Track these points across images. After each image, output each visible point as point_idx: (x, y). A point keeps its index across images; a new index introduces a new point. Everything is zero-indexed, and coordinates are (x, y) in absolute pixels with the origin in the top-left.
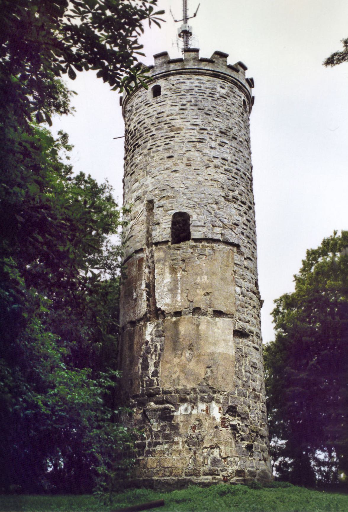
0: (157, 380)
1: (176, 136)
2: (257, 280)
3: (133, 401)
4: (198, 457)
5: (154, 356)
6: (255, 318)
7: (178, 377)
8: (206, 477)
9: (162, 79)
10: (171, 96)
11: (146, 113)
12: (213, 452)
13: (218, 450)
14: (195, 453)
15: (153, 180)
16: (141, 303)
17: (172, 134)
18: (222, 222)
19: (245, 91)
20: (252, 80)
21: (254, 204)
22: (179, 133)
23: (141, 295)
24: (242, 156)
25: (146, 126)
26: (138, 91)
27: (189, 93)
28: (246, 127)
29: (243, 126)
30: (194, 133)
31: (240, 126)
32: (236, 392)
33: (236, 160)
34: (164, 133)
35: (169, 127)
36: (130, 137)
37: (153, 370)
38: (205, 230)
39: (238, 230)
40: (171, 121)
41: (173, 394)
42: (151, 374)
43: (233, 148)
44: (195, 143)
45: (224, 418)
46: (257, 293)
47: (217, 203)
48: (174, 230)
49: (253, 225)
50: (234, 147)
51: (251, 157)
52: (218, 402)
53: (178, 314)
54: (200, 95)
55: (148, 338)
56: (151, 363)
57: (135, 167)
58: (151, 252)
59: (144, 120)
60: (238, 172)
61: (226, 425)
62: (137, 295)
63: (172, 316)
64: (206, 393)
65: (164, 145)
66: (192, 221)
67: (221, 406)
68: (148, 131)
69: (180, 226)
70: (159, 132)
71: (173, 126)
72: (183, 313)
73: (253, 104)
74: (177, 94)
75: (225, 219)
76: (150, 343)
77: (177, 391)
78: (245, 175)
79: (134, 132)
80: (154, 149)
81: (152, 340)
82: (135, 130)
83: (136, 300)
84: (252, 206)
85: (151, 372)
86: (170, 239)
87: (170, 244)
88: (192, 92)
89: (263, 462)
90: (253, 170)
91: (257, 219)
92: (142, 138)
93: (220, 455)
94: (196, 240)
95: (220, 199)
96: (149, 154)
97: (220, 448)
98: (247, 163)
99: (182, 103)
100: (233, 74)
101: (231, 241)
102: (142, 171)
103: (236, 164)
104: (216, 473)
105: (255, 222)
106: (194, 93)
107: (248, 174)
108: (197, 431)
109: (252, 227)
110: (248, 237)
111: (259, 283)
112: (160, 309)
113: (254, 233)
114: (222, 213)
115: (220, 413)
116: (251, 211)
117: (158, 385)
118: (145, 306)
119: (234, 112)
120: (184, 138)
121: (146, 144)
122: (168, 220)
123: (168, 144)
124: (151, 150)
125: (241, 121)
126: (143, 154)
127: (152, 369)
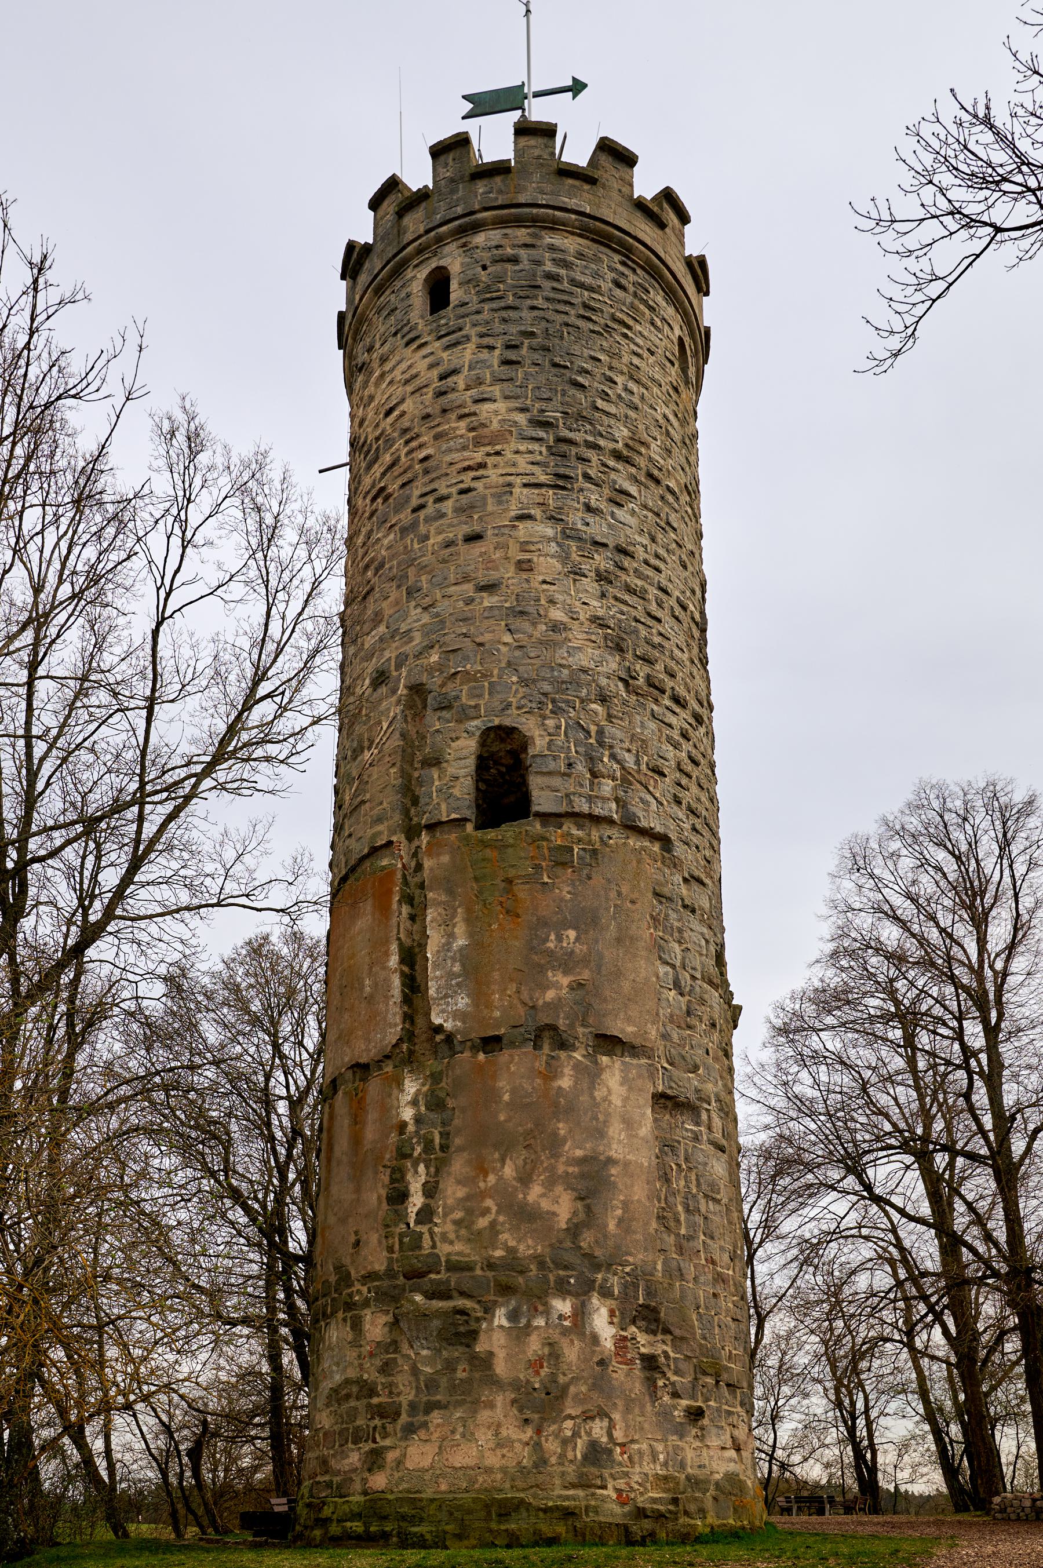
0: (431, 1233)
1: (490, 461)
2: (723, 946)
3: (365, 1289)
4: (547, 1440)
5: (421, 1168)
6: (716, 1059)
7: (493, 1224)
8: (571, 1492)
9: (455, 244)
10: (478, 312)
11: (407, 376)
12: (591, 1428)
13: (605, 1423)
14: (539, 1432)
15: (426, 619)
16: (387, 1011)
17: (478, 456)
18: (618, 762)
19: (682, 304)
20: (702, 261)
21: (711, 708)
22: (498, 453)
23: (387, 981)
24: (674, 545)
25: (407, 424)
26: (387, 293)
27: (529, 302)
28: (688, 442)
29: (677, 437)
30: (541, 453)
31: (668, 433)
32: (659, 1267)
33: (657, 556)
34: (458, 450)
35: (472, 429)
36: (363, 465)
37: (419, 1205)
38: (570, 786)
39: (664, 787)
40: (474, 408)
41: (478, 1272)
42: (413, 1215)
43: (650, 514)
44: (543, 491)
45: (625, 1338)
46: (720, 983)
47: (603, 699)
48: (482, 786)
49: (707, 776)
50: (651, 510)
51: (701, 549)
52: (606, 1293)
53: (491, 1043)
54: (557, 311)
55: (407, 1114)
56: (416, 1185)
57: (377, 570)
58: (415, 855)
59: (403, 401)
60: (664, 597)
61: (629, 1356)
62: (376, 985)
63: (475, 1049)
64: (573, 1269)
65: (455, 496)
66: (534, 756)
67: (612, 1303)
68: (414, 444)
69: (499, 772)
70: (444, 447)
71: (483, 425)
72: (505, 1041)
73: (706, 361)
74: (495, 305)
75: (626, 755)
76: (411, 1128)
77: (490, 1266)
78: (684, 608)
79: (375, 447)
80: (430, 510)
81: (418, 1120)
82: (377, 439)
83: (370, 1000)
84: (704, 712)
85: (415, 1210)
86: (470, 813)
87: (469, 827)
88: (536, 297)
89: (732, 1453)
90: (707, 595)
91: (718, 756)
92: (397, 471)
93: (610, 1435)
94: (546, 818)
95: (613, 688)
96: (414, 525)
97: (610, 1419)
98: (690, 568)
99: (507, 337)
100: (645, 230)
101: (644, 824)
102: (394, 584)
103: (658, 570)
104: (598, 1482)
105: (712, 766)
106: (540, 302)
107: (691, 607)
108: (545, 1371)
109: (704, 782)
110: (692, 811)
111: (728, 956)
112: (439, 1029)
113: (713, 799)
114: (619, 734)
115: (611, 1323)
116: (702, 730)
117: (434, 1246)
118: (398, 1019)
119: (653, 380)
120: (513, 470)
121: (407, 490)
122: (465, 752)
123: (468, 490)
124: (422, 514)
125: (671, 417)
126: (397, 528)
127: (416, 1201)
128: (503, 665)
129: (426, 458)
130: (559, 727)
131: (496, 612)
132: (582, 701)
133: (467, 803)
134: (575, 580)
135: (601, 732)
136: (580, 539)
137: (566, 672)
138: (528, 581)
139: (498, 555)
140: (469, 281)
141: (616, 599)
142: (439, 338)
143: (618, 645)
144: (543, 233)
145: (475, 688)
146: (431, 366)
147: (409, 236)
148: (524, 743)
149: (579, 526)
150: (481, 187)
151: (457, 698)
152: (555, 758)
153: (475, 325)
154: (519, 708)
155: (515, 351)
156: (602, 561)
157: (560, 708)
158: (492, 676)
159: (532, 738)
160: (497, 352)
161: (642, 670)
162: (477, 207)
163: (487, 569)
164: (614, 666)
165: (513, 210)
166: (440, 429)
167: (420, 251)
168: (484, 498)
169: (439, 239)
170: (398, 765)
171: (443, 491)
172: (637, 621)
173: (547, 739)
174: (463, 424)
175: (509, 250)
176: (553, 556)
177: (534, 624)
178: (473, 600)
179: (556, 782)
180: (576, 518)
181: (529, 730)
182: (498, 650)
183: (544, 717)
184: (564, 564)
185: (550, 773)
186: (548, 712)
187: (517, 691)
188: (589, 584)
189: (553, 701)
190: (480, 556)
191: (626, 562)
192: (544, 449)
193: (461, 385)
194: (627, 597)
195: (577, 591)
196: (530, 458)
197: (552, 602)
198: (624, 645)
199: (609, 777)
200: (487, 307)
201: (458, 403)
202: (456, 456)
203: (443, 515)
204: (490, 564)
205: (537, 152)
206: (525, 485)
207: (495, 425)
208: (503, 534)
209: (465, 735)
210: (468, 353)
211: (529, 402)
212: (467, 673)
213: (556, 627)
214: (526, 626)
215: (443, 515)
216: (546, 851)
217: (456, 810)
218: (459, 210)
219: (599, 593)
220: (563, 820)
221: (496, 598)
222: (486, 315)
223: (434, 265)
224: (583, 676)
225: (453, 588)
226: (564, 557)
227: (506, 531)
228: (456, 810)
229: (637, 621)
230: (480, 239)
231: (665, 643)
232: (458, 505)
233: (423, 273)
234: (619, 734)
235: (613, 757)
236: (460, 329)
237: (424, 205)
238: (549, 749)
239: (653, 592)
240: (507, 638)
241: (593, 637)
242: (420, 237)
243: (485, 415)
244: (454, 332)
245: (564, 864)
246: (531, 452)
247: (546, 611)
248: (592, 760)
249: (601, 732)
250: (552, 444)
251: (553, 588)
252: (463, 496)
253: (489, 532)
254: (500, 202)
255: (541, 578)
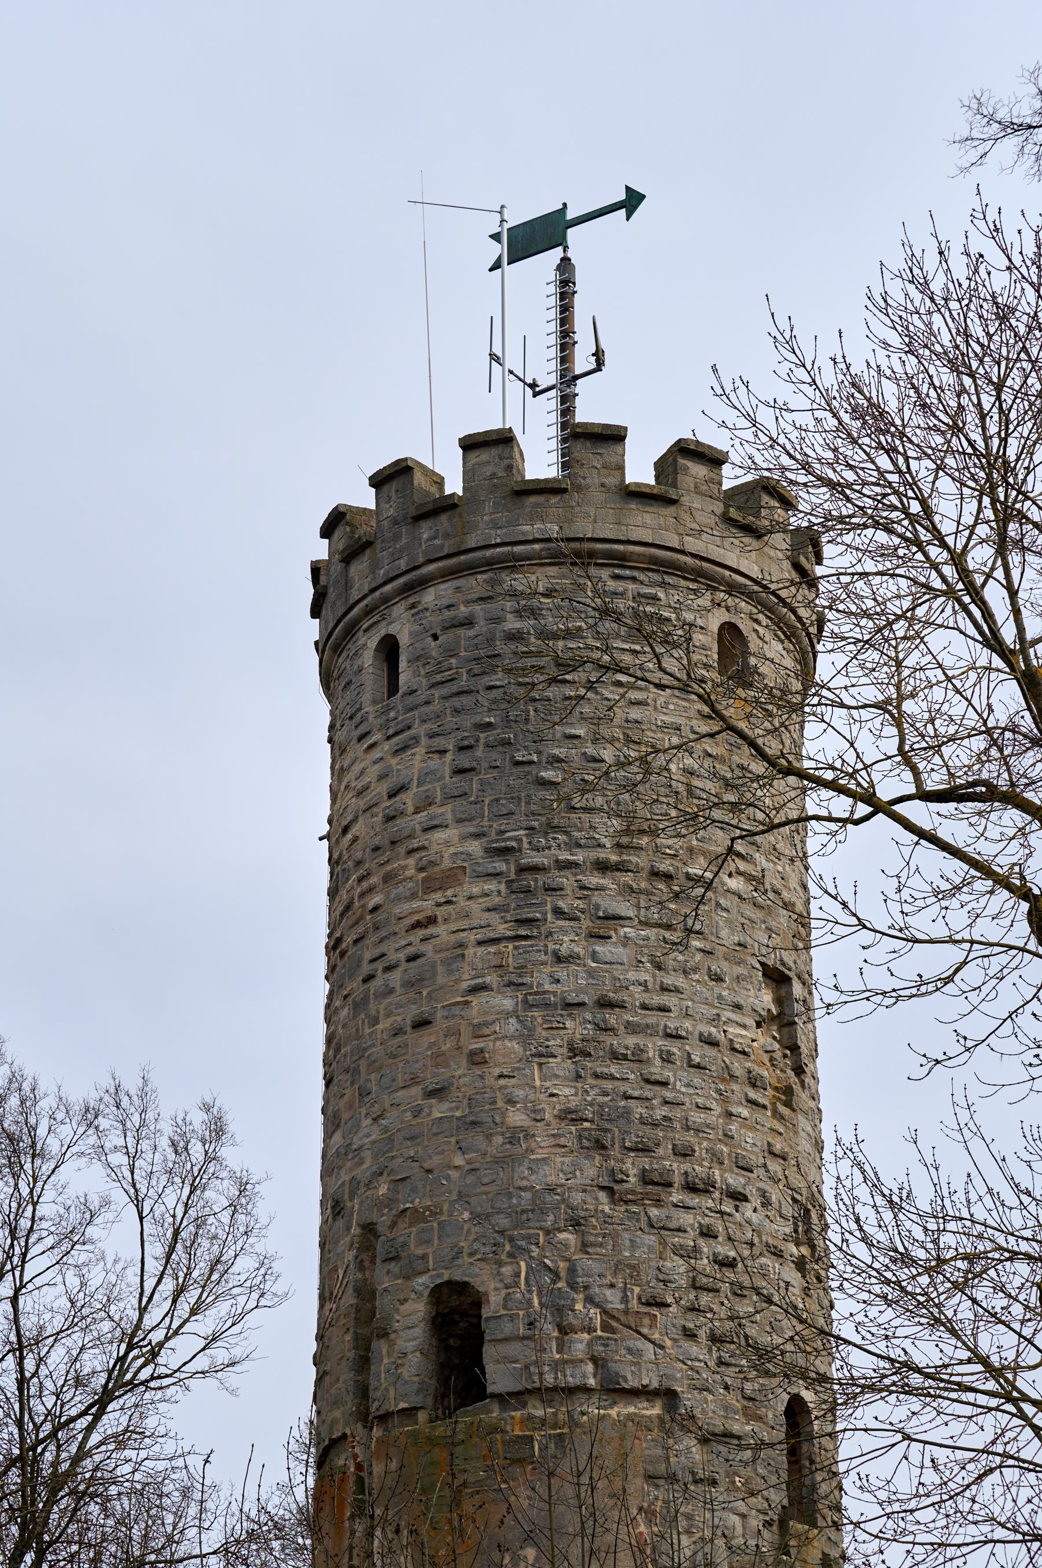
1: (441, 912)
10: (427, 703)
18: (597, 1305)
35: (422, 869)
44: (501, 946)
47: (576, 1224)
66: (488, 1319)
71: (432, 863)
74: (445, 690)
75: (608, 1293)
94: (501, 1398)
101: (632, 1383)
106: (498, 678)
120: (464, 924)
128: (454, 1197)
129: (375, 909)
130: (518, 1275)
131: (446, 1125)
132: (548, 1232)
133: (416, 1386)
134: (540, 1065)
135: (572, 1271)
136: (547, 1005)
137: (526, 1195)
138: (482, 1077)
139: (448, 1046)
140: (418, 659)
141: (596, 1076)
142: (389, 738)
143: (597, 1141)
144: (503, 575)
145: (423, 1231)
146: (381, 777)
147: (355, 595)
148: (477, 1302)
149: (547, 987)
150: (426, 530)
151: (405, 1245)
152: (512, 1318)
153: (424, 721)
154: (471, 1255)
155: (469, 753)
156: (576, 1028)
157: (520, 1248)
158: (441, 1213)
159: (486, 1294)
160: (449, 756)
161: (632, 1167)
162: (421, 560)
163: (436, 1066)
164: (592, 1172)
165: (462, 557)
166: (389, 868)
167: (368, 612)
168: (433, 966)
169: (386, 600)
170: (352, 1330)
171: (393, 957)
172: (627, 1097)
173: (504, 1292)
174: (411, 861)
175: (462, 608)
176: (512, 1038)
177: (489, 1137)
178: (420, 1111)
179: (514, 1349)
180: (541, 978)
181: (483, 1283)
182: (448, 1178)
183: (500, 1264)
184: (525, 1045)
185: (506, 1340)
186: (504, 1257)
187: (469, 1231)
188: (560, 1065)
189: (511, 1240)
190: (429, 1048)
191: (612, 1018)
192: (503, 887)
193: (410, 809)
194: (614, 1069)
195: (543, 1079)
196: (485, 902)
197: (511, 1102)
198: (607, 1141)
199: (583, 1330)
200: (437, 693)
201: (407, 832)
202: (406, 907)
203: (391, 991)
204: (440, 1059)
205: (488, 470)
206: (480, 943)
207: (447, 863)
208: (454, 1016)
209: (413, 1296)
210: (417, 760)
211: (485, 823)
212: (416, 1210)
213: (514, 1136)
214: (480, 1141)
215: (391, 991)
216: (500, 1446)
217: (404, 1397)
218: (403, 564)
219: (573, 1074)
220: (526, 1396)
221: (446, 1106)
222: (436, 706)
223: (383, 633)
224: (548, 1198)
225: (401, 1093)
226: (526, 1037)
227: (456, 1010)
228: (404, 1397)
229: (627, 1097)
230: (429, 597)
231: (677, 1113)
232: (406, 978)
233: (373, 643)
234: (595, 1266)
235: (589, 1300)
236: (409, 728)
237: (368, 552)
238: (505, 1307)
239: (653, 1046)
240: (459, 1160)
241: (562, 1141)
242: (365, 597)
243: (435, 848)
244: (402, 731)
245: (520, 1461)
246: (486, 895)
247: (504, 1115)
248: (559, 1310)
249: (572, 1271)
250: (513, 876)
251: (513, 1081)
252: (412, 964)
253: (439, 1014)
254: (446, 552)
255: (497, 1071)
